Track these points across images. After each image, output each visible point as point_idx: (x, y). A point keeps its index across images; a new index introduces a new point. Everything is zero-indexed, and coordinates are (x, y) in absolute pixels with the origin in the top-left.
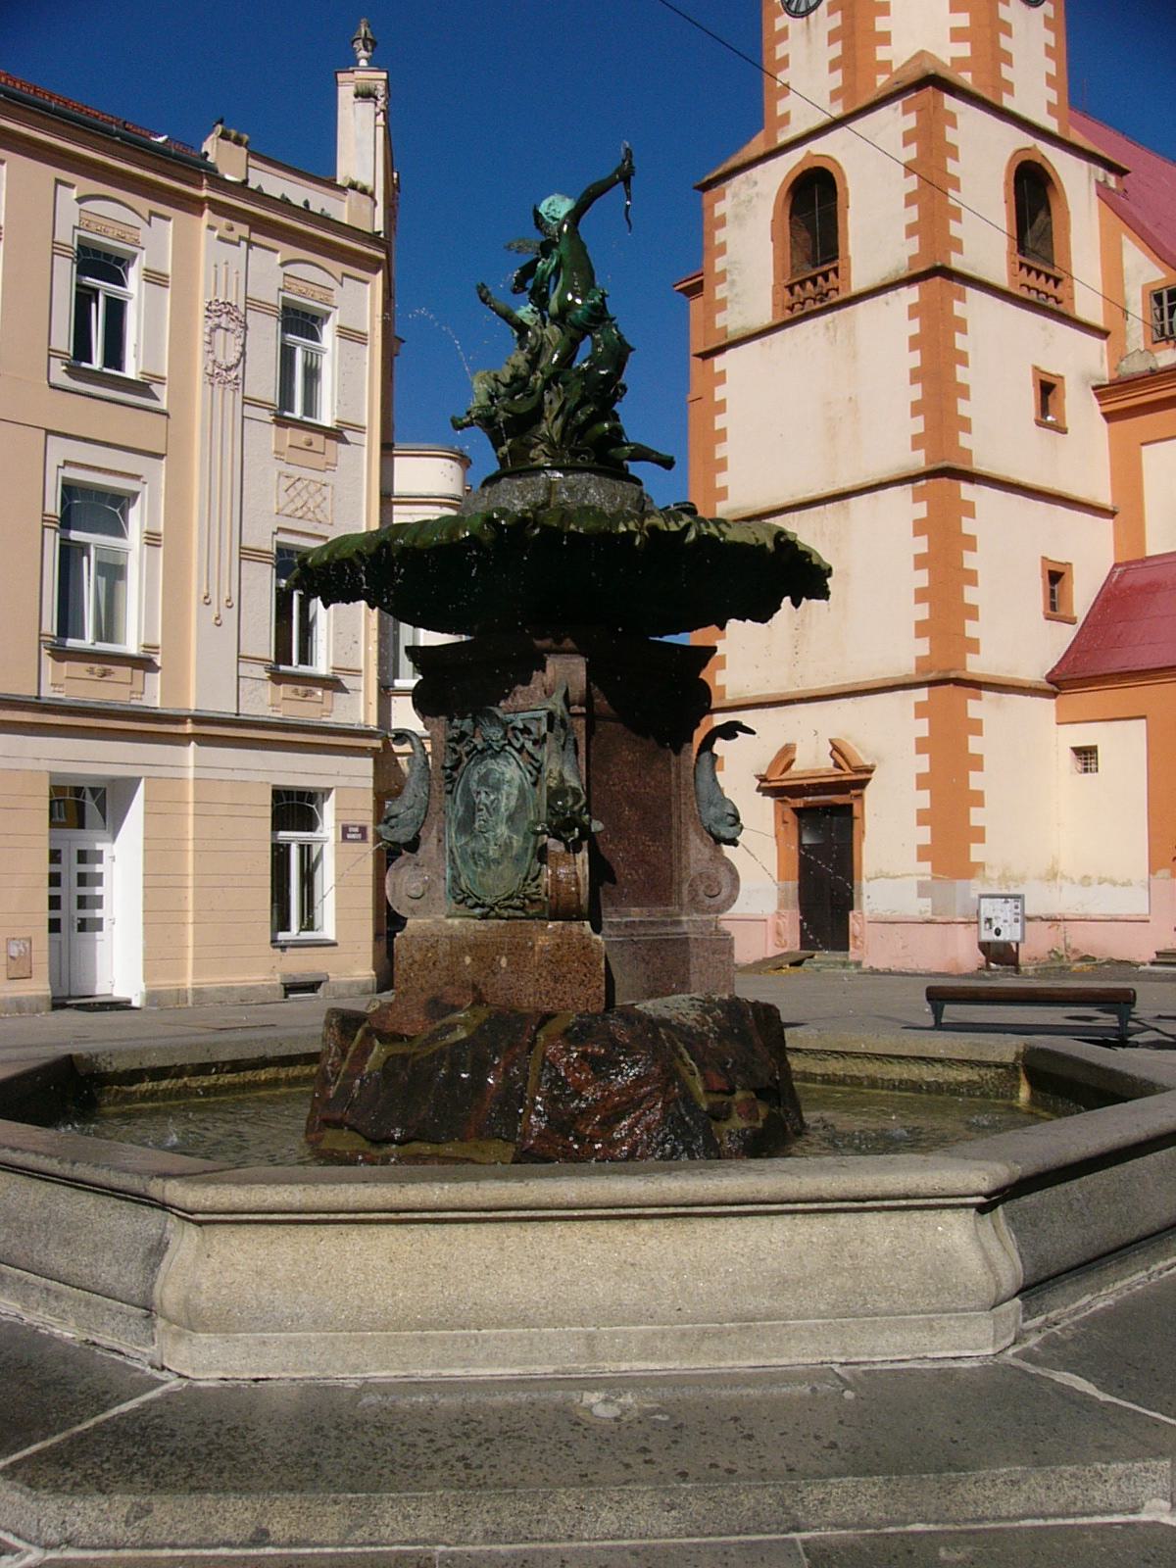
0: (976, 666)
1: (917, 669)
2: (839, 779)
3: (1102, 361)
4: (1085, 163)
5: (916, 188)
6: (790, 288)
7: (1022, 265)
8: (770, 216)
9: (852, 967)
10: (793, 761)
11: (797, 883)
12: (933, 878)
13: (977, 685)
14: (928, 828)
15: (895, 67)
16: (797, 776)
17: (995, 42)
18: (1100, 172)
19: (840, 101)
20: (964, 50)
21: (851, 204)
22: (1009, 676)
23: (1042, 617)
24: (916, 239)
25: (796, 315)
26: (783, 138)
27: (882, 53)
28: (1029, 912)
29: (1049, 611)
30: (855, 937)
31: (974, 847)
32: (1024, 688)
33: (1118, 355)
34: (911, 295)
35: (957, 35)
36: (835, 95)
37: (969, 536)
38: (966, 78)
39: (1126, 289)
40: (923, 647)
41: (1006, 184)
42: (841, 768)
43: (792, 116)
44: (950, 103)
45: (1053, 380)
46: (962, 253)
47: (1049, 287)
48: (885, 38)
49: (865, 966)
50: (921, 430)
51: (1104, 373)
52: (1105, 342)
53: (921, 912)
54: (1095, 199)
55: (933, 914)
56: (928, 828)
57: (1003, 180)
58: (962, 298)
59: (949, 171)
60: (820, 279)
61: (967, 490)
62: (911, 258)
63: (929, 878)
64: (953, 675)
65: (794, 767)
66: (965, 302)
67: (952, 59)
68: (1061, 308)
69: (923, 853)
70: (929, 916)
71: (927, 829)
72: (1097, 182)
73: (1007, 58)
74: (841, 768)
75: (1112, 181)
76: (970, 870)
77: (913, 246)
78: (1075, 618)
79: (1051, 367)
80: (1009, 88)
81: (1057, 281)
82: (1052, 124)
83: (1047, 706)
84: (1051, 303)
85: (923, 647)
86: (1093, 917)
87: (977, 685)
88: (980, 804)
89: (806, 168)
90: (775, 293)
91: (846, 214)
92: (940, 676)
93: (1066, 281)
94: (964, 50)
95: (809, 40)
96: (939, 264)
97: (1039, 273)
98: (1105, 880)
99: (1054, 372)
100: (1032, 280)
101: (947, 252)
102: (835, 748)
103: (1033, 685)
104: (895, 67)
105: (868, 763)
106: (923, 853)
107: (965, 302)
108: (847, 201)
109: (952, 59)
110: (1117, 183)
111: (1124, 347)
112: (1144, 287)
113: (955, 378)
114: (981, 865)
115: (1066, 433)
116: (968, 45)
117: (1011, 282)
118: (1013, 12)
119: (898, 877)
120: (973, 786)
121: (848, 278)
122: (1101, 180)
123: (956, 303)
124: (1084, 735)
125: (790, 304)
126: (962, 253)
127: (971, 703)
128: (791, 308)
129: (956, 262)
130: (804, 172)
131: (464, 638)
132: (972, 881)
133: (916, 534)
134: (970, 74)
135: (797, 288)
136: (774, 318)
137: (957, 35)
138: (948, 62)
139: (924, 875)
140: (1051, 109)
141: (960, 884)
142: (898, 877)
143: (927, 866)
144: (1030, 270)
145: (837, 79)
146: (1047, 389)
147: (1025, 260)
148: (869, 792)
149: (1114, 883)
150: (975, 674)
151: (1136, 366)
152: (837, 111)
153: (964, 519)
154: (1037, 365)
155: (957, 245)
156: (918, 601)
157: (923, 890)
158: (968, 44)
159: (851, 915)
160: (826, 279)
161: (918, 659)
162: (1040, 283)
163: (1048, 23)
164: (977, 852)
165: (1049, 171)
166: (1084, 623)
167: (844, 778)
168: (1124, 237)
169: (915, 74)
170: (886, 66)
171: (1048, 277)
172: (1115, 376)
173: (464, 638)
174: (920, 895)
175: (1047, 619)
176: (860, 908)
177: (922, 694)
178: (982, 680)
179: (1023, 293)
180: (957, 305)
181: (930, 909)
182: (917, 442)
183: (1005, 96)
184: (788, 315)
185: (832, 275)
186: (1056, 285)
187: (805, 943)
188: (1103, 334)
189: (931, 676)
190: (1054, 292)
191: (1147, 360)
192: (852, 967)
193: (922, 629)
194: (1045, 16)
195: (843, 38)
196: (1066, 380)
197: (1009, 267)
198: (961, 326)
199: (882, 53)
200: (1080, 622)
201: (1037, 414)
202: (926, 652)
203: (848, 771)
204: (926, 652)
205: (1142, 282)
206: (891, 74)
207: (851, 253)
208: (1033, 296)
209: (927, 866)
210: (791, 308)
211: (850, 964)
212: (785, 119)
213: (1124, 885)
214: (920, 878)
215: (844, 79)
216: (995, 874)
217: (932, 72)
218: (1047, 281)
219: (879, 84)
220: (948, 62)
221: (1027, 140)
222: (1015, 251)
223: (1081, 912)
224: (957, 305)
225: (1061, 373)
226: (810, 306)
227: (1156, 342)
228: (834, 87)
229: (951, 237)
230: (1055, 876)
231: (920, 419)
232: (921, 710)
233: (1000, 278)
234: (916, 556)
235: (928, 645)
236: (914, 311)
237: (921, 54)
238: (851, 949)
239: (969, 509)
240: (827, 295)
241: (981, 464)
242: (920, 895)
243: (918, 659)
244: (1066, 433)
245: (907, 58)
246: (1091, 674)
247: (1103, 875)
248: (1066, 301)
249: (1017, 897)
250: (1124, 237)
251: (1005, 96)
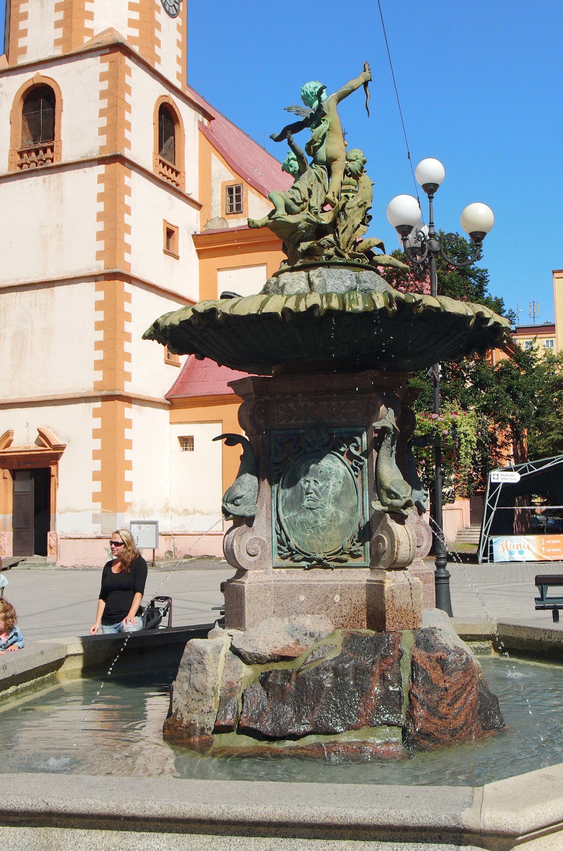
0: (129, 389)
1: (94, 388)
2: (43, 452)
3: (197, 221)
4: (194, 111)
5: (106, 107)
6: (21, 154)
7: (160, 161)
8: (10, 107)
9: (51, 566)
10: (12, 441)
11: (12, 515)
12: (102, 512)
13: (129, 400)
14: (100, 482)
15: (95, 33)
16: (14, 450)
17: (153, 33)
18: (201, 117)
19: (61, 47)
20: (135, 33)
21: (64, 109)
22: (147, 395)
23: (163, 362)
24: (105, 137)
25: (23, 170)
26: (22, 61)
27: (88, 24)
28: (161, 530)
29: (167, 359)
30: (51, 548)
31: (127, 493)
32: (154, 402)
33: (206, 220)
34: (101, 169)
35: (132, 23)
36: (57, 42)
37: (128, 313)
38: (136, 49)
39: (212, 184)
40: (99, 376)
41: (155, 114)
42: (45, 446)
43: (28, 50)
44: (128, 62)
45: (173, 229)
46: (130, 149)
47: (173, 176)
48: (90, 16)
49: (58, 565)
50: (103, 249)
51: (198, 229)
52: (199, 212)
53: (95, 533)
54: (197, 131)
55: (102, 533)
56: (100, 482)
57: (153, 111)
58: (130, 176)
59: (126, 100)
60: (41, 152)
61: (127, 287)
62: (101, 148)
63: (100, 512)
64: (118, 393)
65: (12, 445)
66: (131, 178)
67: (128, 36)
68: (178, 188)
69: (96, 497)
70: (99, 534)
71: (99, 483)
72: (199, 121)
73: (158, 43)
74: (45, 446)
75: (206, 122)
76: (125, 507)
77: (103, 140)
78: (180, 364)
79: (173, 222)
80: (158, 59)
81: (177, 173)
82: (178, 84)
83: (164, 414)
84: (174, 184)
85: (99, 376)
86: (190, 533)
87: (129, 400)
88: (130, 468)
89: (35, 82)
90: (11, 155)
91: (60, 114)
92: (110, 393)
93: (182, 174)
94: (135, 33)
95: (42, 6)
96: (119, 153)
97: (168, 167)
98: (197, 511)
99: (174, 224)
100: (164, 170)
101: (122, 147)
102: (41, 434)
103: (159, 401)
104: (95, 33)
105: (61, 443)
106: (96, 497)
107: (131, 178)
108: (62, 107)
109: (128, 36)
110: (208, 124)
111: (210, 214)
112: (223, 183)
113: (124, 222)
114: (129, 504)
115: (178, 259)
116: (138, 30)
117: (154, 170)
118: (161, 17)
119: (80, 511)
120: (127, 458)
121: (60, 153)
122: (201, 120)
123: (126, 177)
124: (186, 430)
125: (20, 163)
126: (130, 149)
127: (127, 410)
128: (21, 166)
129: (128, 154)
130: (34, 85)
131: (247, 438)
132: (125, 513)
133: (96, 309)
134: (138, 47)
135: (25, 155)
136: (9, 170)
137: (132, 23)
138: (126, 38)
139: (96, 510)
140: (179, 76)
141: (119, 515)
142: (80, 511)
143: (99, 505)
144: (164, 164)
145: (59, 33)
146: (170, 233)
147: (162, 159)
148: (61, 462)
149: (202, 513)
150: (129, 393)
151: (216, 226)
152: (59, 52)
153: (125, 303)
154: (166, 219)
155: (128, 144)
156: (96, 349)
157: (96, 518)
158: (138, 30)
159: (48, 534)
160: (45, 152)
161: (95, 383)
162: (169, 173)
163: (179, 28)
164: (128, 497)
165: (176, 110)
166: (184, 367)
167: (46, 452)
168: (212, 154)
169: (108, 40)
170: (90, 32)
171: (173, 170)
172: (204, 229)
173: (247, 438)
174: (94, 522)
175: (166, 363)
176: (55, 530)
177: (98, 405)
178: (133, 396)
179: (160, 177)
180: (127, 179)
181: (100, 530)
182: (99, 255)
183: (156, 64)
184: (18, 170)
185: (49, 151)
186: (176, 176)
187: (15, 553)
188: (199, 206)
189: (104, 393)
190: (176, 179)
191: (223, 223)
192: (51, 566)
193: (98, 365)
194: (177, 24)
195: (65, 10)
196: (180, 229)
197: (153, 161)
198: (128, 191)
199: (88, 24)
200: (182, 366)
201: (164, 247)
202: (101, 379)
203: (49, 448)
204: (101, 379)
205: (222, 180)
206: (93, 37)
207: (63, 138)
208: (164, 179)
209: (99, 505)
210: (21, 166)
211: (49, 564)
212: (24, 50)
213: (208, 514)
214: (95, 512)
215: (64, 34)
216: (137, 509)
217: (120, 41)
218: (168, 169)
219: (85, 41)
220: (126, 38)
221: (165, 91)
222: (157, 153)
223: (181, 531)
224: (127, 179)
225: (178, 225)
226: (33, 166)
227: (227, 214)
228: (58, 37)
229: (125, 139)
230: (168, 509)
231: (102, 243)
232: (96, 413)
233: (150, 167)
234: (96, 322)
235: (102, 375)
236: (101, 179)
237: (111, 30)
238: (49, 555)
239: (128, 297)
240: (45, 162)
241: (134, 273)
242: (94, 522)
243: (95, 383)
244: (178, 259)
245: (102, 30)
246: (191, 395)
247: (196, 509)
248: (181, 185)
249: (155, 523)
250: (212, 154)
251: (156, 64)
